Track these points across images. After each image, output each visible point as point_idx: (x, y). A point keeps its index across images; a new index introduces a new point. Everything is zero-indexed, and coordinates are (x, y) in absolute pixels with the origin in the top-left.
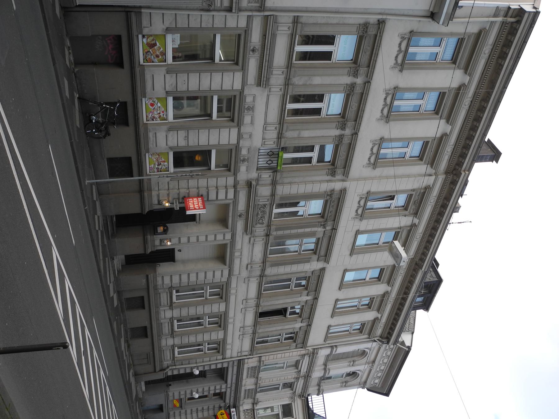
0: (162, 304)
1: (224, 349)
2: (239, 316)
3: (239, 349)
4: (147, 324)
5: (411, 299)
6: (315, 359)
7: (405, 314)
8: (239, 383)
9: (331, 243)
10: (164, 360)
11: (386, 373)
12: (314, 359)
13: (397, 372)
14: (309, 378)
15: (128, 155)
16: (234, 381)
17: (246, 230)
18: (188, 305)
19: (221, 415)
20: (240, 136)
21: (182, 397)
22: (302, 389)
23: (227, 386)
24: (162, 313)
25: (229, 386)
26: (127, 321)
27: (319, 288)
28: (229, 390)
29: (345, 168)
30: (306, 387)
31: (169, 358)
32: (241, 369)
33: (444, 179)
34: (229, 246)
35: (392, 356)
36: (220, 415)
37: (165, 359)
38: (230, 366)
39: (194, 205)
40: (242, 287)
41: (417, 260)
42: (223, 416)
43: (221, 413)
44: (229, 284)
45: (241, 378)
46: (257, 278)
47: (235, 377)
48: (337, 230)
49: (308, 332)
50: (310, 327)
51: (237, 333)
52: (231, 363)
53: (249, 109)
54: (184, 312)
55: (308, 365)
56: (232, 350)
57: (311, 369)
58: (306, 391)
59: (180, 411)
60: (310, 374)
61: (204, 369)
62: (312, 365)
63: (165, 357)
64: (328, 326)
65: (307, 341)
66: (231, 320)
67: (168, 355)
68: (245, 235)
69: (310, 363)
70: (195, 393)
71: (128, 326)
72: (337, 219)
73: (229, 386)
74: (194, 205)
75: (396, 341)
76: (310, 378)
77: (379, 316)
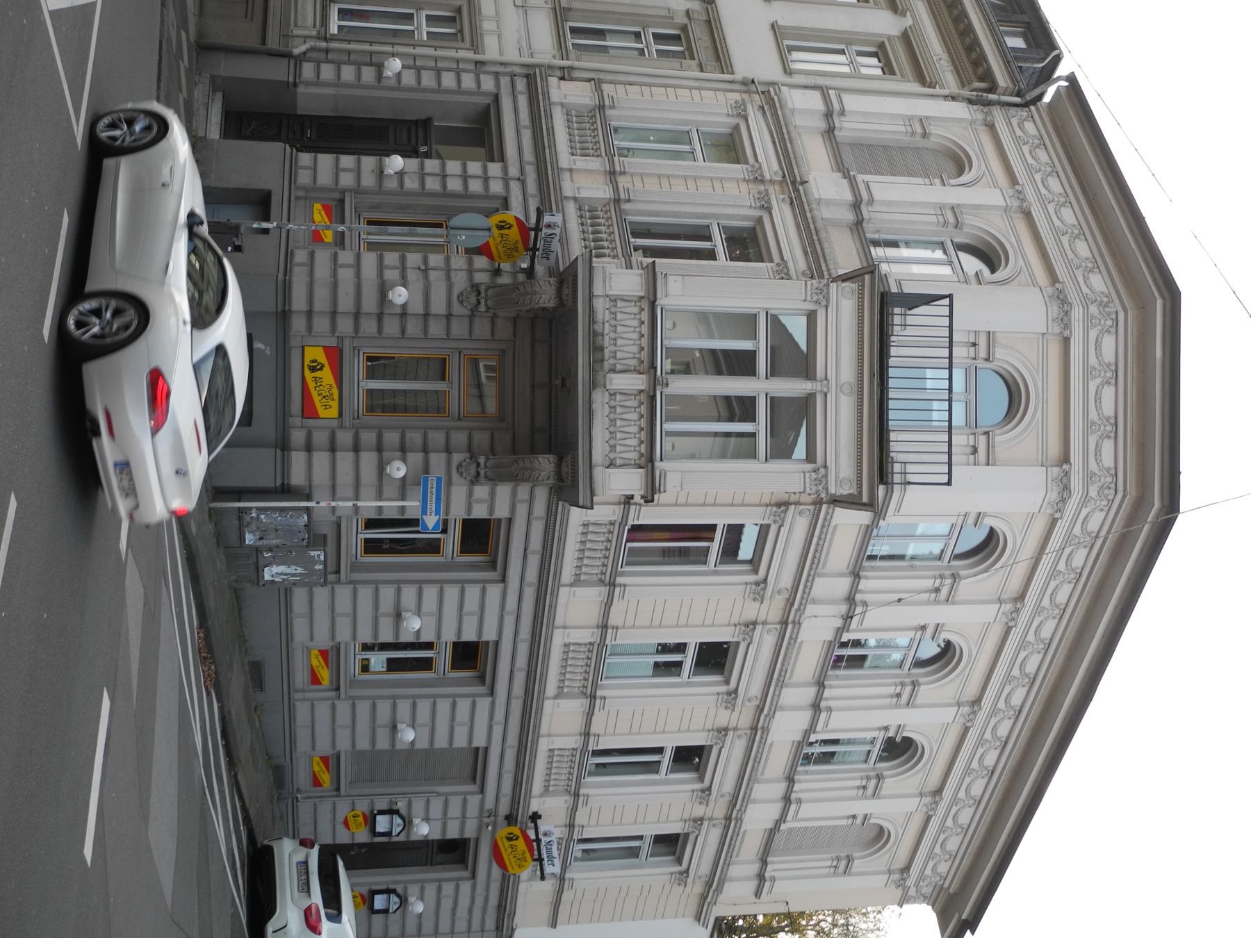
1: (474, 32)
6: (791, 143)
8: (547, 151)
12: (779, 112)
14: (801, 188)
16: (529, 155)
19: (509, 839)
22: (806, 253)
23: (505, 170)
25: (513, 171)
27: (721, 44)
28: (522, 510)
29: (718, 59)
30: (814, 232)
31: (310, 22)
32: (540, 97)
35: (1071, 187)
36: (505, 841)
37: (299, 23)
38: (502, 91)
42: (514, 843)
43: (509, 834)
46: (576, 738)
47: (527, 135)
49: (715, 20)
50: (713, 5)
52: (505, 81)
55: (774, 143)
56: (499, 36)
57: (781, 116)
58: (822, 249)
60: (796, 171)
61: (376, 640)
62: (786, 136)
63: (299, 17)
65: (717, 17)
69: (774, 131)
73: (513, 171)
76: (805, 185)
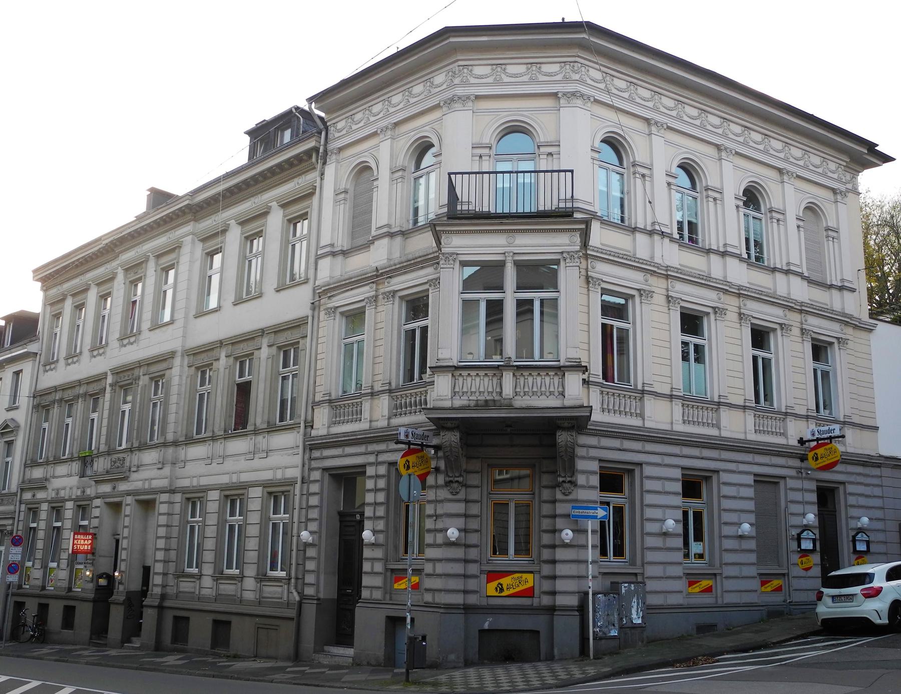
0: (193, 590)
2: (229, 465)
3: (286, 454)
4: (210, 618)
5: (231, 180)
7: (269, 162)
8: (359, 437)
9: (287, 325)
10: (281, 598)
11: (408, 80)
13: (396, 61)
15: (61, 609)
16: (361, 449)
17: (125, 479)
18: (241, 550)
20: (70, 500)
21: (753, 571)
22: (422, 268)
23: (371, 464)
24: (204, 592)
25: (372, 459)
26: (200, 648)
30: (409, 263)
33: (174, 230)
34: (137, 498)
37: (279, 596)
38: (320, 466)
39: (84, 545)
40: (192, 469)
41: (189, 217)
44: (185, 490)
45: (344, 437)
47: (349, 450)
48: (221, 341)
51: (257, 463)
52: (314, 464)
53: (57, 494)
54: (209, 556)
55: (352, 289)
56: (152, 479)
59: (725, 578)
60: (369, 275)
63: (276, 596)
64: (278, 294)
66: (279, 475)
67: (271, 590)
68: (131, 479)
70: (739, 530)
71: (207, 649)
72: (246, 336)
73: (372, 459)
74: (84, 545)
75: (300, 140)
76: (379, 268)
77: (274, 204)
